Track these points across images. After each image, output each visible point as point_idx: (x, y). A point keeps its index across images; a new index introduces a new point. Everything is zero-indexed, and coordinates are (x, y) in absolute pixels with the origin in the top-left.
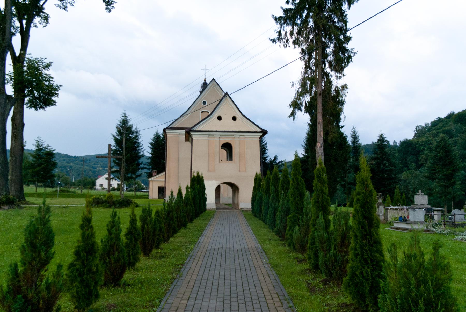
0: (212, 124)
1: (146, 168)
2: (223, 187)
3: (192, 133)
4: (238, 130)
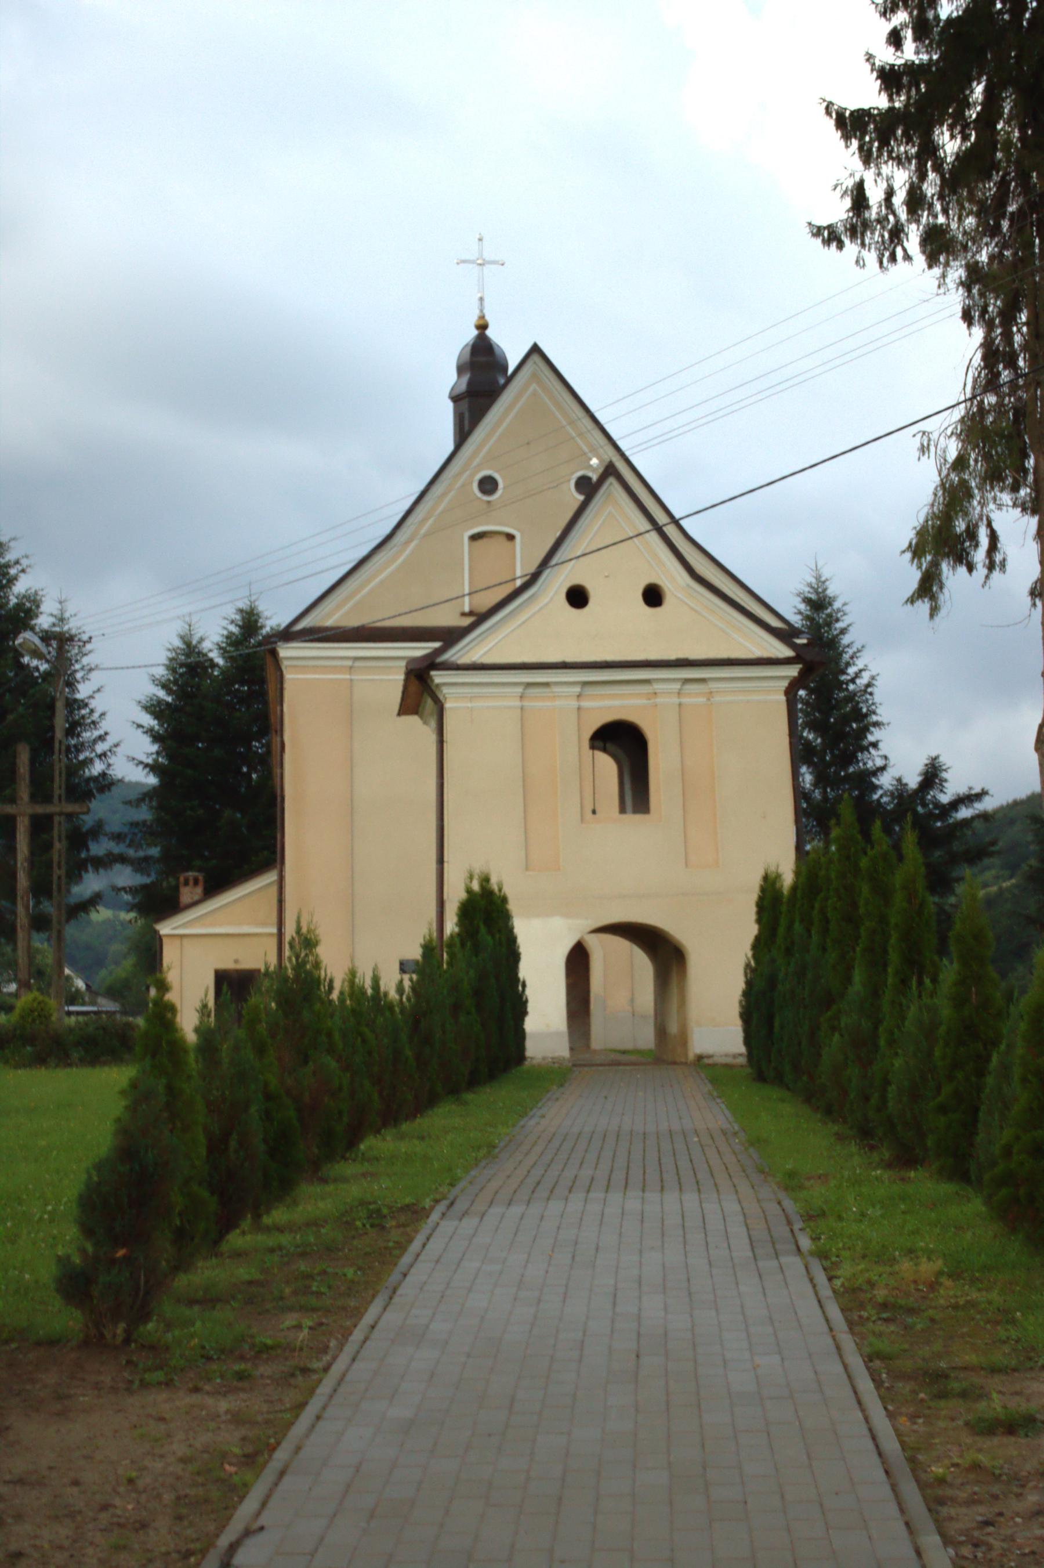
0: (541, 628)
1: (122, 859)
2: (600, 949)
3: (438, 677)
4: (672, 656)
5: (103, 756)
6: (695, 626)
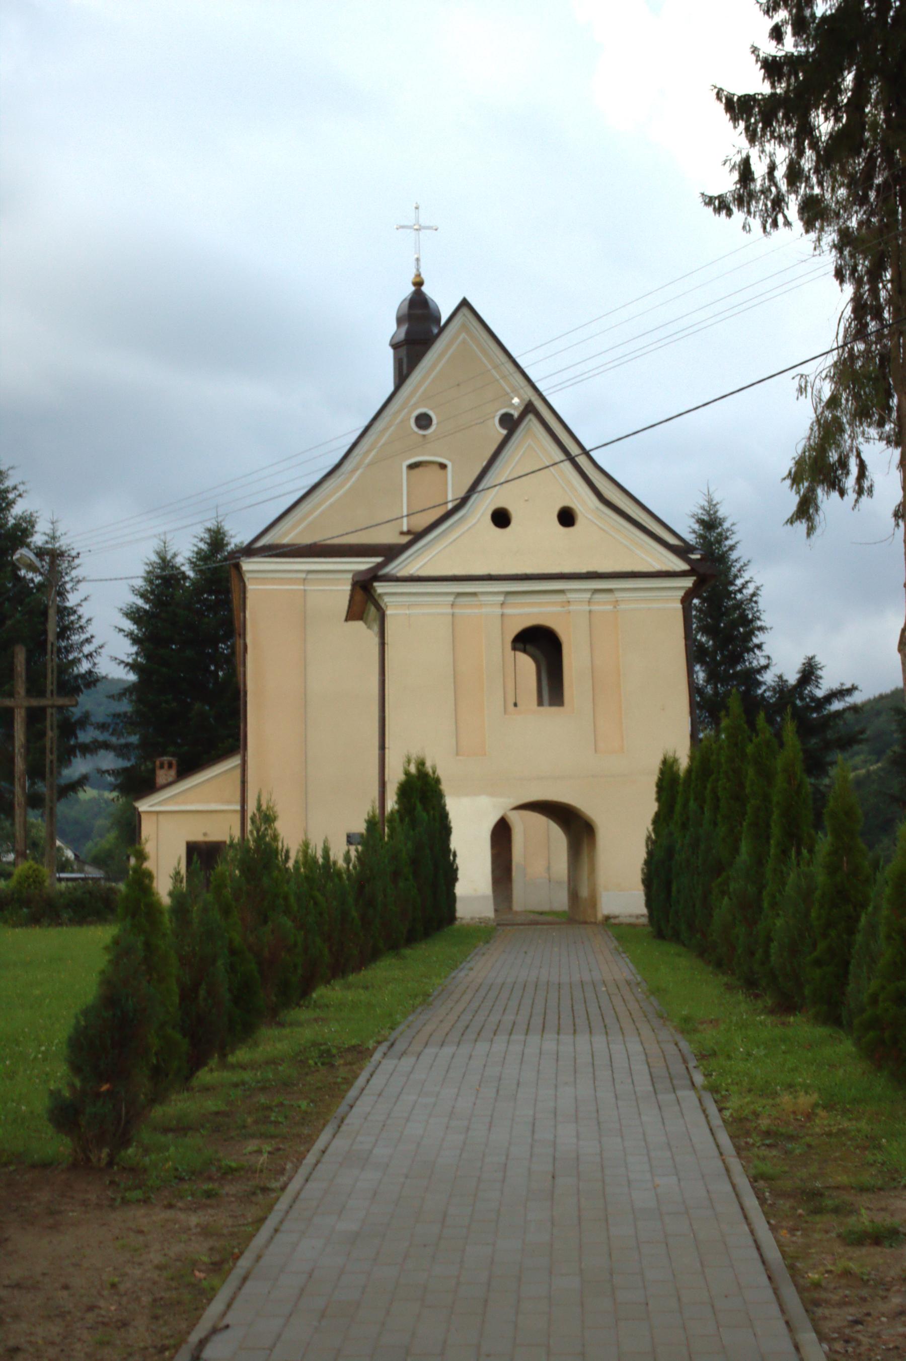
0: (469, 545)
1: (106, 746)
2: (521, 823)
3: (380, 588)
4: (583, 569)
5: (89, 656)
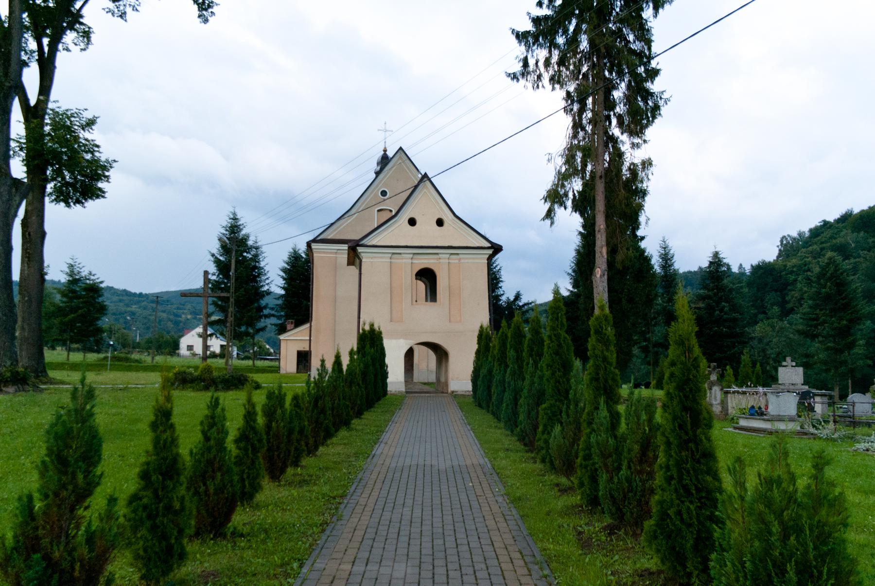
0: (398, 233)
1: (273, 315)
2: (419, 352)
3: (360, 249)
4: (447, 245)
6: (451, 235)
